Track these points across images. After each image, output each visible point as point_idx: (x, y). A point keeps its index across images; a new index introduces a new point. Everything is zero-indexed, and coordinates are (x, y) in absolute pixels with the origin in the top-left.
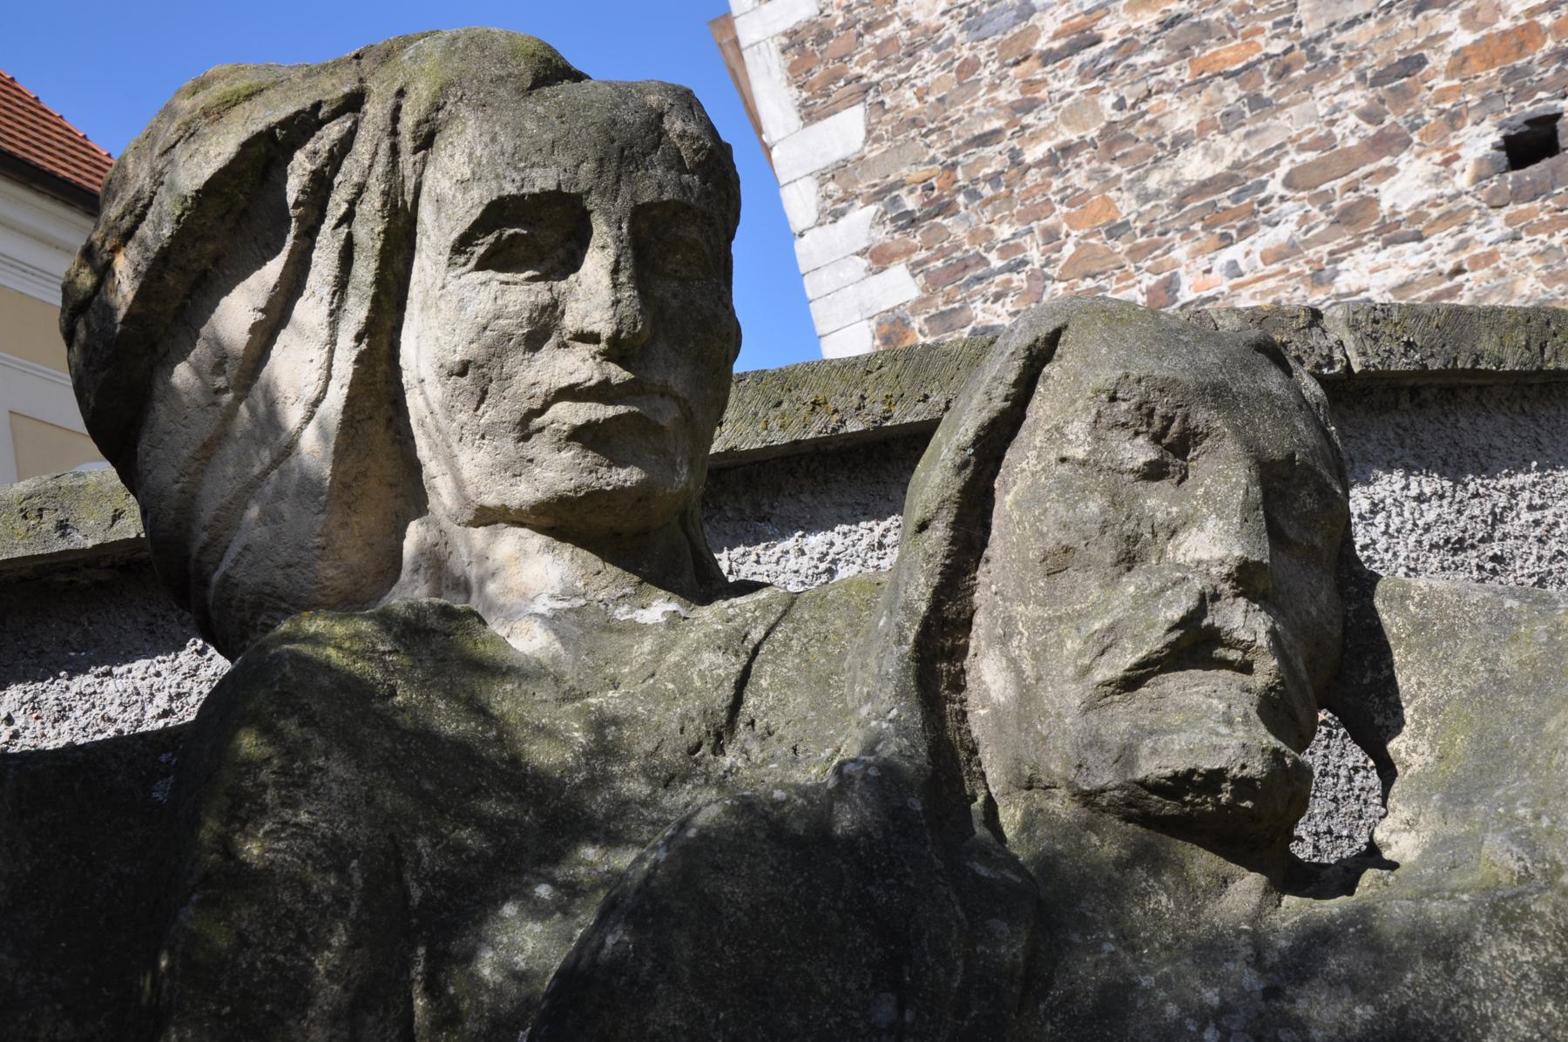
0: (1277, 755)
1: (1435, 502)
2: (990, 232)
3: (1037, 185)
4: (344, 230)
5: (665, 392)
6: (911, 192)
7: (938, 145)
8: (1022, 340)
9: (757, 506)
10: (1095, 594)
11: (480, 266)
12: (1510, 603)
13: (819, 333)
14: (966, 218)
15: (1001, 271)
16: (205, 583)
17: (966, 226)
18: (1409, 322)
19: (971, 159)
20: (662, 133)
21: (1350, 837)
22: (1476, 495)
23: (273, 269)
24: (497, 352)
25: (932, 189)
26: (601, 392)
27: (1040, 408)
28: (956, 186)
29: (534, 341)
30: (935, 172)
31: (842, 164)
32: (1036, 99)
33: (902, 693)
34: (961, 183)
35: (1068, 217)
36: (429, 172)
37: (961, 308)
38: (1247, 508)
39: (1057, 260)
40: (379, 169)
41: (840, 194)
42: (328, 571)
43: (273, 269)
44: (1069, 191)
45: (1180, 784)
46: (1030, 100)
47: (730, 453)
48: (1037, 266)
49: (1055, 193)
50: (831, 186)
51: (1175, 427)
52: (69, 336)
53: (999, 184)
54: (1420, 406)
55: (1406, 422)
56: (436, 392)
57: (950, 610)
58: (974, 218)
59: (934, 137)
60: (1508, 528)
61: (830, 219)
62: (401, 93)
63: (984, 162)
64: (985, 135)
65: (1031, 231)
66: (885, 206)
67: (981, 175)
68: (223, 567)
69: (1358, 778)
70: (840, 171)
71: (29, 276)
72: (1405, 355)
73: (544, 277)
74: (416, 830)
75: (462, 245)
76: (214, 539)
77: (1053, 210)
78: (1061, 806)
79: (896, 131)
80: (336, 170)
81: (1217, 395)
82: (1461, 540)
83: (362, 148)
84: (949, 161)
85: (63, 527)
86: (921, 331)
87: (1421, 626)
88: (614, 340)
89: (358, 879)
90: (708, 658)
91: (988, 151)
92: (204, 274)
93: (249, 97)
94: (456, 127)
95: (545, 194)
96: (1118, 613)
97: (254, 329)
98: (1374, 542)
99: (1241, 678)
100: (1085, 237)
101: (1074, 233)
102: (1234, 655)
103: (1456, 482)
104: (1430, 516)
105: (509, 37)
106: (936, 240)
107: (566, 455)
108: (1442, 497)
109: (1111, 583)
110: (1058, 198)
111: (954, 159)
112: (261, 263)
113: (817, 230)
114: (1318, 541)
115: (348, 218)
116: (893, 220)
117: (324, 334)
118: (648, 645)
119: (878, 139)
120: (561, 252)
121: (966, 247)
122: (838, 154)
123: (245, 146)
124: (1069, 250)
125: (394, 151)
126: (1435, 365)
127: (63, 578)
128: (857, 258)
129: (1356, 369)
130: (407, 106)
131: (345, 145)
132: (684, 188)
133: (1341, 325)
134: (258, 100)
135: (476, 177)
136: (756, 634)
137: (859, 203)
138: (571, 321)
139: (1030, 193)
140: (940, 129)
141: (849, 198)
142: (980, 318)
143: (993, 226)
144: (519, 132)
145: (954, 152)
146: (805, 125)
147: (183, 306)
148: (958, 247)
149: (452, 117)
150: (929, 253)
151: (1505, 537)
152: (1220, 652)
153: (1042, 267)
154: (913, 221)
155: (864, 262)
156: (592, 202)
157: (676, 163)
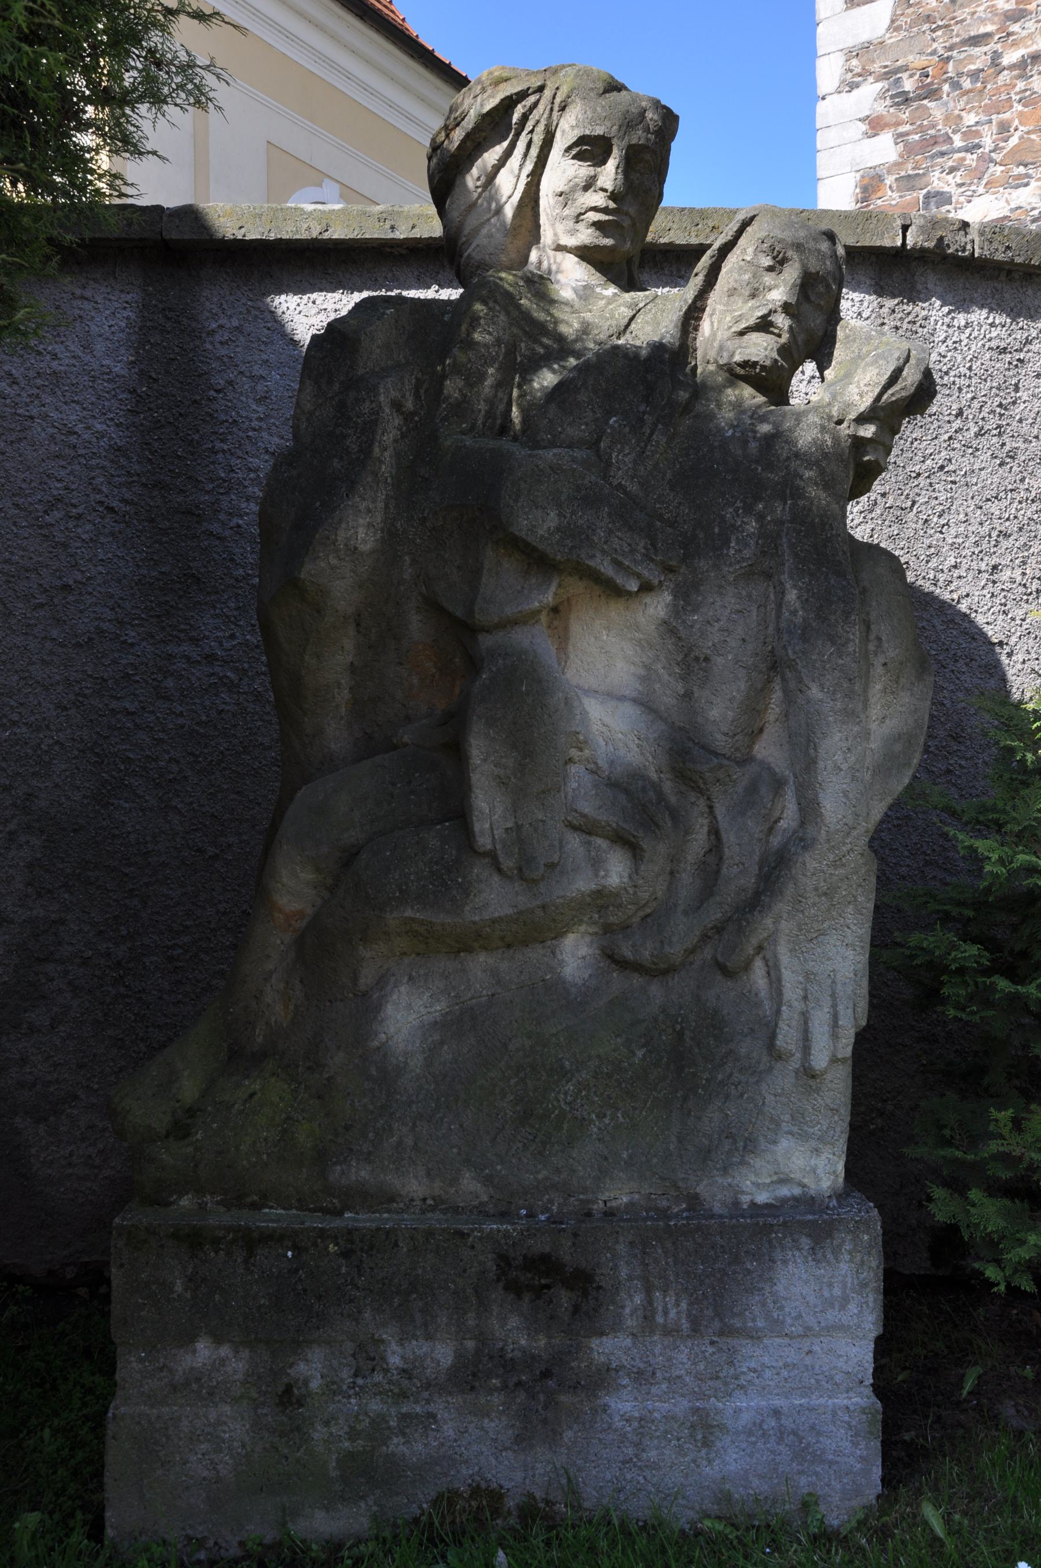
0: (776, 361)
1: (999, 328)
2: (960, 117)
3: (1005, 85)
4: (530, 136)
5: (627, 214)
6: (911, 76)
7: (941, 40)
8: (741, 217)
9: (679, 270)
10: (740, 304)
11: (573, 158)
12: (873, 333)
13: (819, 177)
14: (946, 104)
15: (959, 150)
16: (461, 256)
17: (944, 110)
18: (1013, 236)
19: (963, 56)
20: (644, 117)
21: (904, 467)
22: (1022, 329)
23: (505, 144)
24: (573, 190)
25: (927, 76)
26: (605, 210)
27: (742, 241)
28: (945, 76)
29: (586, 188)
30: (933, 63)
31: (867, 45)
32: (1026, 10)
33: (676, 326)
34: (949, 75)
35: (1021, 114)
36: (562, 120)
37: (924, 174)
38: (794, 285)
39: (1003, 148)
40: (545, 116)
41: (858, 70)
42: (503, 258)
43: (505, 144)
44: (1028, 93)
45: (745, 364)
46: (1021, 10)
47: (671, 244)
48: (987, 150)
49: (1016, 94)
50: (854, 62)
51: (781, 255)
52: (430, 159)
53: (977, 80)
54: (1010, 280)
55: (999, 287)
56: (552, 201)
57: (699, 304)
58: (951, 104)
59: (939, 33)
60: (1032, 347)
61: (847, 89)
62: (557, 88)
63: (971, 59)
64: (978, 36)
65: (990, 122)
66: (889, 85)
67: (966, 70)
68: (469, 251)
69: (916, 443)
70: (863, 51)
71: (239, 7)
72: (1004, 253)
73: (593, 166)
74: (521, 341)
75: (568, 149)
76: (467, 240)
77: (1011, 107)
78: (712, 367)
79: (914, 23)
80: (531, 113)
81: (798, 247)
82: (1005, 349)
83: (541, 107)
84: (946, 55)
85: (393, 228)
86: (890, 187)
87: (847, 337)
88: (612, 192)
89: (503, 350)
90: (623, 309)
91: (977, 51)
92: (480, 143)
93: (506, 80)
94: (574, 105)
95: (599, 136)
96: (744, 311)
97: (493, 166)
98: (961, 341)
99: (776, 338)
100: (1028, 133)
101: (1021, 128)
102: (776, 331)
103: (1013, 320)
104: (994, 334)
105: (599, 72)
106: (919, 117)
107: (590, 231)
108: (1003, 326)
109: (746, 302)
110: (1018, 97)
111: (950, 53)
112: (500, 142)
113: (835, 95)
114: (822, 303)
115: (532, 132)
116: (892, 97)
117: (517, 172)
118: (603, 302)
119: (898, 29)
120: (601, 158)
121: (940, 127)
122: (865, 37)
123: (502, 100)
124: (1014, 141)
125: (552, 109)
126: (1019, 260)
127: (388, 250)
128: (859, 123)
129: (976, 255)
130: (559, 94)
131: (535, 105)
132: (648, 140)
133: (976, 232)
134: (509, 82)
135: (577, 126)
136: (641, 305)
137: (871, 79)
138: (600, 183)
139: (998, 91)
140: (946, 26)
141: (865, 74)
142: (935, 184)
143: (963, 114)
144: (594, 111)
145: (951, 48)
146: (847, 9)
147: (470, 154)
148: (933, 127)
149: (573, 101)
150: (911, 128)
151: (1029, 351)
152: (772, 329)
153: (991, 152)
154: (907, 100)
155: (864, 127)
156: (614, 141)
157: (647, 130)
